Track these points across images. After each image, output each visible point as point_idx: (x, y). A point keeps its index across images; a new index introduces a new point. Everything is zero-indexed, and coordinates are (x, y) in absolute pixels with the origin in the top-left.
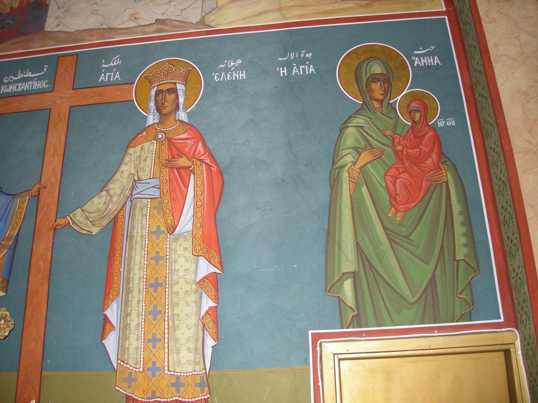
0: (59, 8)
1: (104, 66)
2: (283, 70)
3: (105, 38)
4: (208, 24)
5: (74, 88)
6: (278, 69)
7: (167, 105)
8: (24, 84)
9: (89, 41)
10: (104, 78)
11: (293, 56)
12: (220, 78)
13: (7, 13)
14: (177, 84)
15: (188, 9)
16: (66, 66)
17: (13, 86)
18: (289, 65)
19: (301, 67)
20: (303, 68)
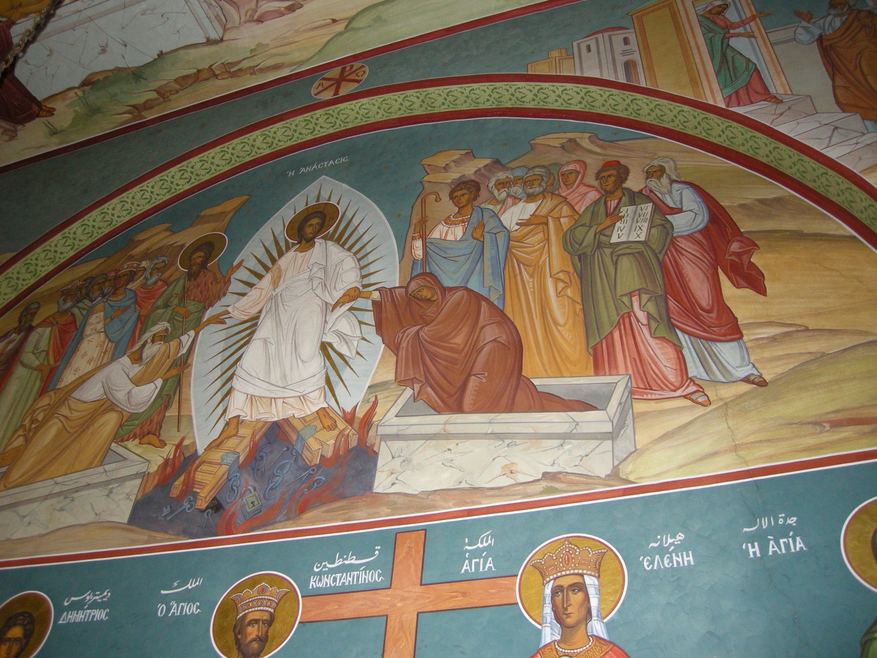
0: (393, 458)
1: (467, 547)
2: (753, 547)
3: (466, 503)
4: (624, 477)
5: (423, 583)
6: (744, 547)
7: (572, 611)
8: (345, 574)
9: (443, 508)
10: (468, 568)
11: (767, 523)
12: (653, 565)
13: (316, 464)
14: (585, 577)
15: (591, 455)
16: (409, 547)
17: (327, 578)
18: (760, 538)
19: (782, 541)
20: (784, 543)
